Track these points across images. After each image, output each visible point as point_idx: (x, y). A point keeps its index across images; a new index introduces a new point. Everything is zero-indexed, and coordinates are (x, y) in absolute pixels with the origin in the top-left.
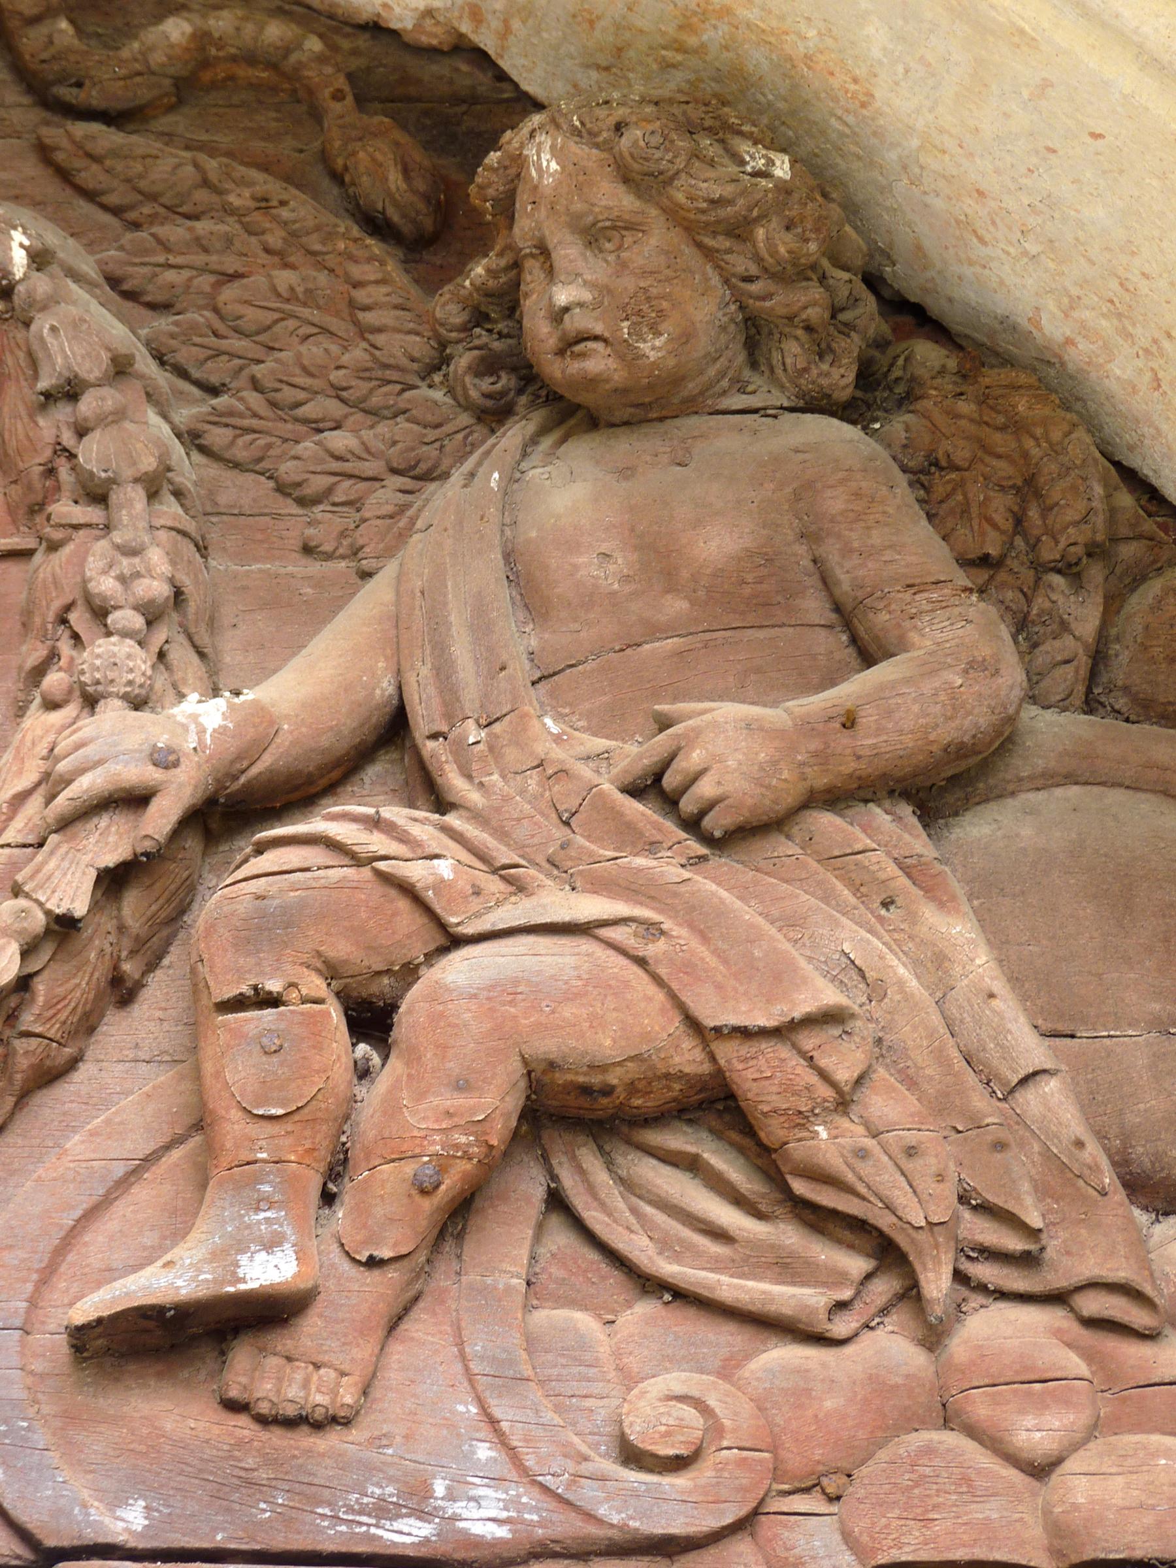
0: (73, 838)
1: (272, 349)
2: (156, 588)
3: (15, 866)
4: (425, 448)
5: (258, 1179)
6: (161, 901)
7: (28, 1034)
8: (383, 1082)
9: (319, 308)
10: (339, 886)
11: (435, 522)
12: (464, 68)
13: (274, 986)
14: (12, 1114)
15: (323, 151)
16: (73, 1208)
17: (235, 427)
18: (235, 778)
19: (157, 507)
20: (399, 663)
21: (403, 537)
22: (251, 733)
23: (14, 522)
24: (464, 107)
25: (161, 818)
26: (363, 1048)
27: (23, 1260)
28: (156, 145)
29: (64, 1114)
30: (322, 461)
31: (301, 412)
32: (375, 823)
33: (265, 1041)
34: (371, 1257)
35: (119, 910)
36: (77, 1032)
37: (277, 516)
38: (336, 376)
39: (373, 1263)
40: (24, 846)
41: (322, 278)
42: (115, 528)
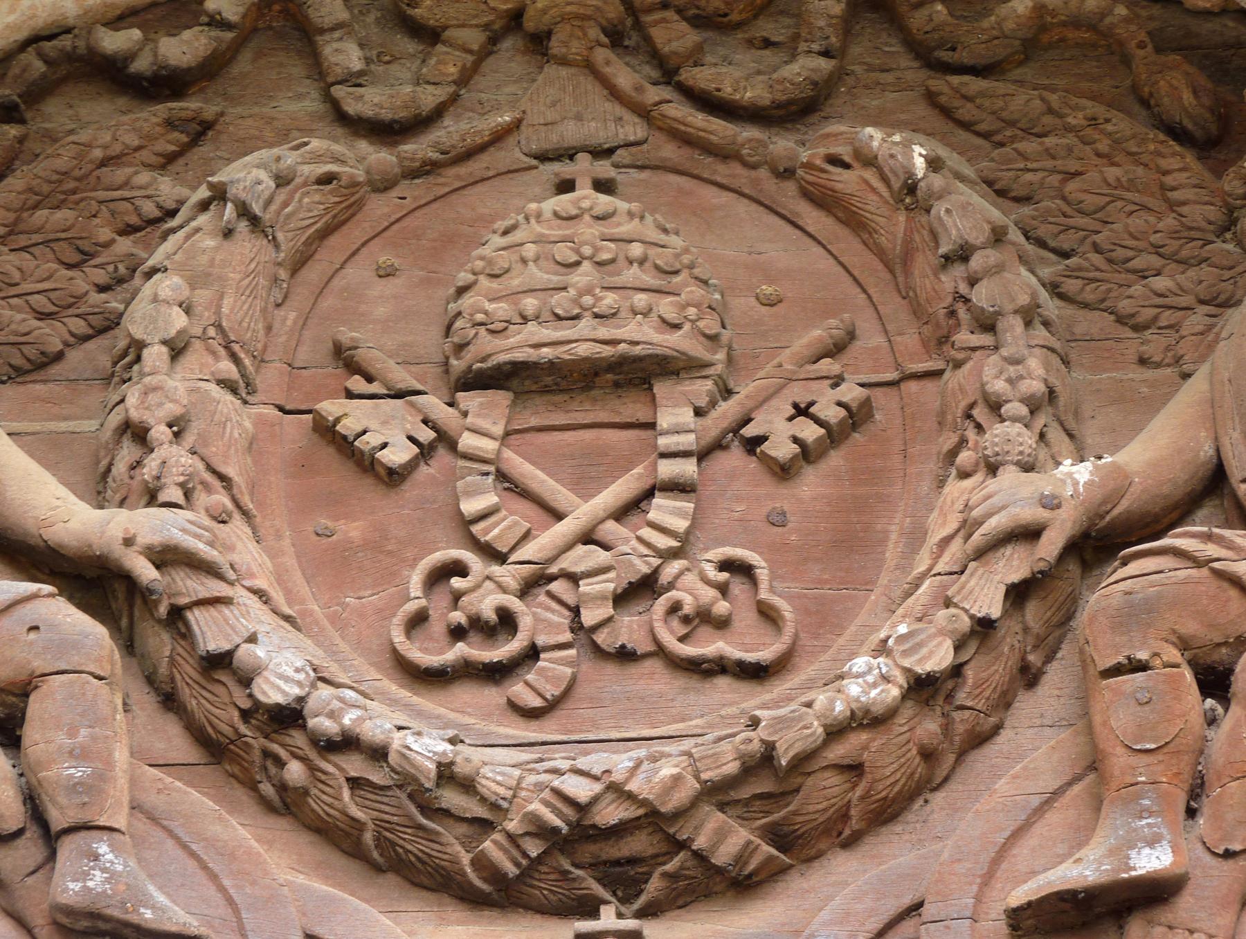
0: (987, 563)
1: (1107, 223)
2: (1035, 386)
3: (946, 587)
4: (1223, 284)
5: (1140, 796)
6: (1053, 609)
7: (962, 708)
8: (1227, 724)
9: (1138, 191)
10: (1185, 582)
11: (1235, 331)
12: (1231, 24)
13: (1142, 655)
14: (953, 769)
15: (1133, 86)
16: (1003, 830)
17: (1083, 278)
18: (1102, 517)
19: (1032, 332)
20: (1216, 433)
21: (1211, 347)
22: (1111, 485)
23: (928, 352)
24: (1233, 51)
25: (1050, 546)
26: (1209, 701)
27: (969, 869)
28: (1011, 88)
29: (992, 766)
30: (1149, 298)
31: (1130, 265)
32: (1209, 537)
33: (1139, 695)
34: (1227, 850)
35: (1023, 616)
36: (998, 706)
37: (1119, 340)
38: (1154, 238)
39: (1228, 855)
40: (951, 574)
41: (1140, 171)
42: (1003, 346)
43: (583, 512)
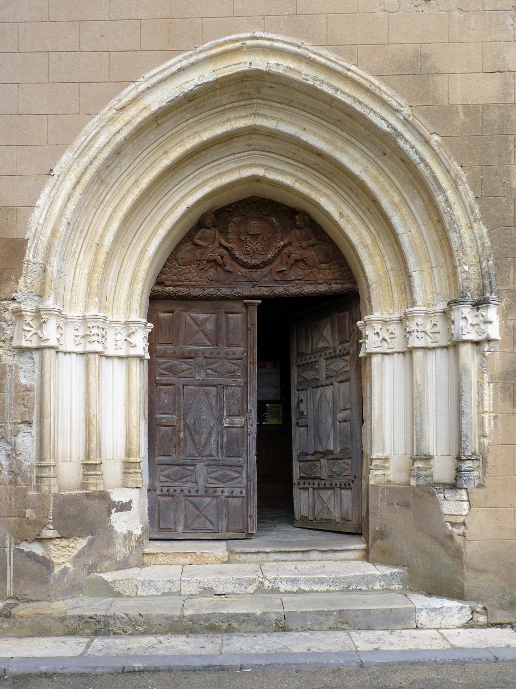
43: (254, 243)
